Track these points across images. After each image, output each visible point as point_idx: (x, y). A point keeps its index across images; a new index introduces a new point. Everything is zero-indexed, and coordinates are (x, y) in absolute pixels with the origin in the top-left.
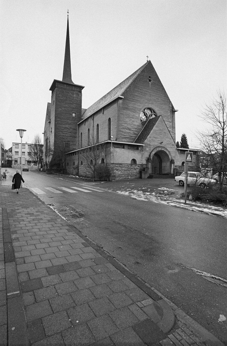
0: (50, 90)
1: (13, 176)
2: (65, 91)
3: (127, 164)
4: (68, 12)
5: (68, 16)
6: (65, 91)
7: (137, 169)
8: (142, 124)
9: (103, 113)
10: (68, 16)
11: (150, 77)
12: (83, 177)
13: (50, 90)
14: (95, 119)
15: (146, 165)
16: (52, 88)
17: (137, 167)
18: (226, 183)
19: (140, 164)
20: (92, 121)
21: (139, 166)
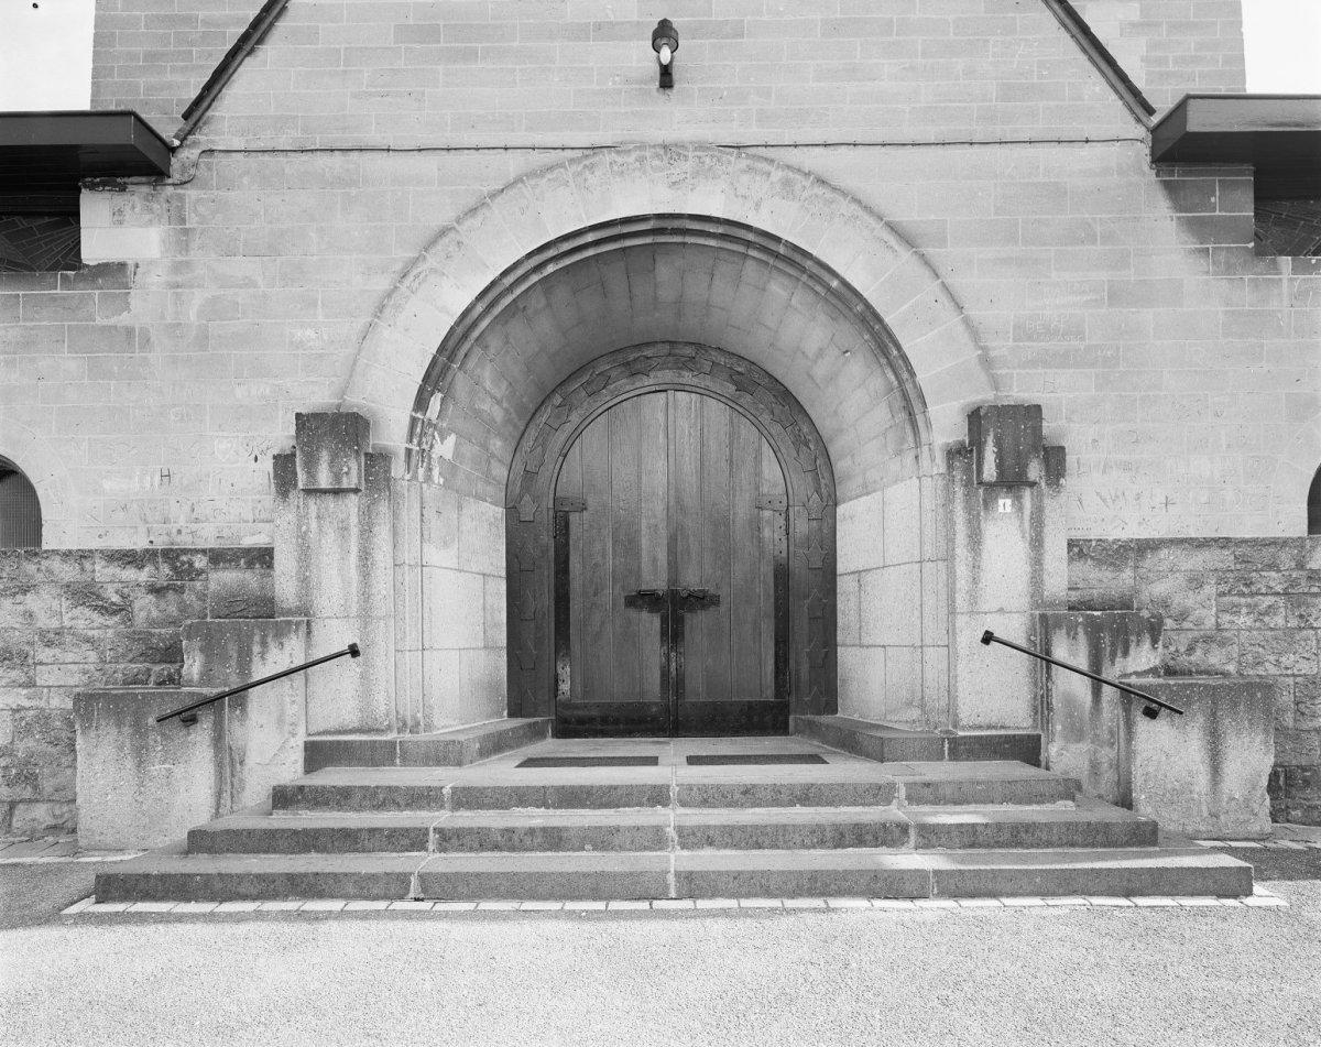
7: (52, 639)
21: (85, 594)
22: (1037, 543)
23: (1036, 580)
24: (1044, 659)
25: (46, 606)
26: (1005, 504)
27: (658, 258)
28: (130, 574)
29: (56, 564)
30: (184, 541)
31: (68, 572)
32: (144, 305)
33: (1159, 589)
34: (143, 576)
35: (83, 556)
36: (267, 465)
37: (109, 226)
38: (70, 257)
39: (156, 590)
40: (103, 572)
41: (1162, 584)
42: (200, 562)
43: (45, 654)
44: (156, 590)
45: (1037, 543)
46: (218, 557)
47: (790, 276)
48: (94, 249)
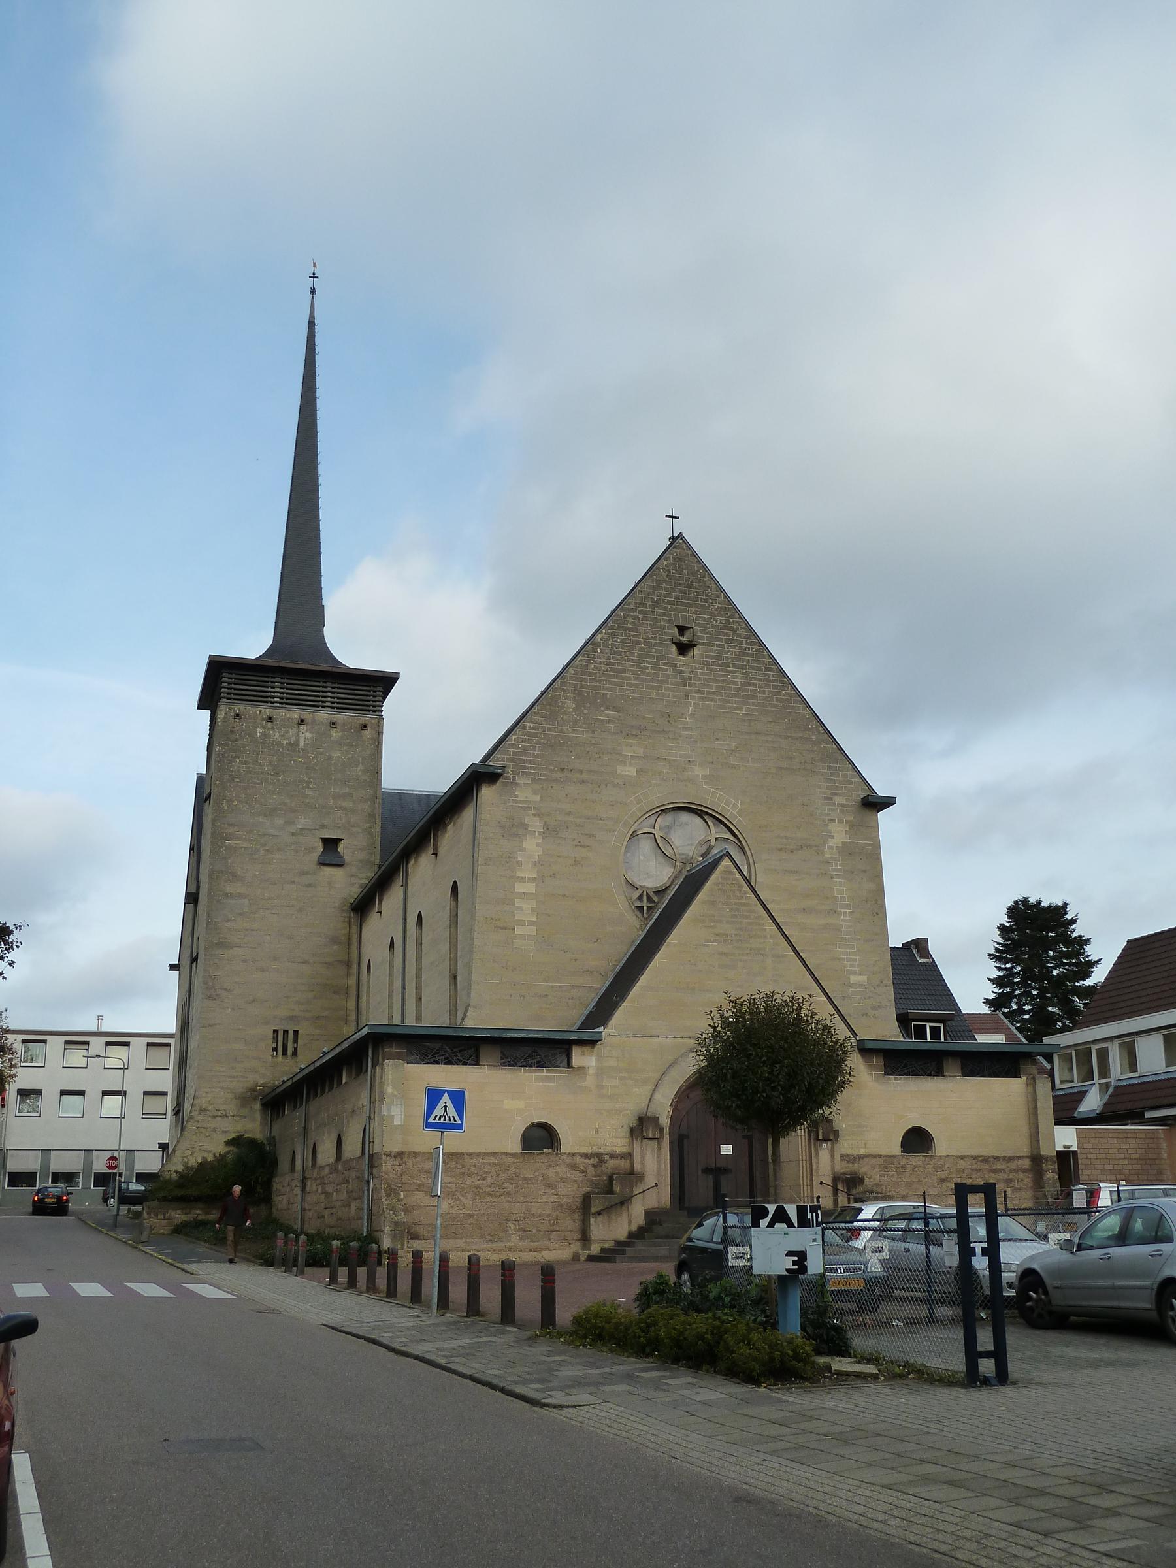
0: (201, 706)
1: (1155, 1287)
2: (288, 686)
3: (493, 1154)
4: (314, 277)
5: (313, 292)
6: (288, 686)
7: (564, 1180)
8: (640, 909)
9: (436, 854)
10: (313, 292)
11: (682, 630)
12: (985, 1252)
13: (201, 706)
14: (442, 850)
15: (623, 1156)
16: (208, 699)
17: (562, 1171)
18: (750, 1259)
19: (583, 1150)
20: (401, 890)
21: (574, 1167)
22: (833, 1156)
23: (833, 1167)
24: (836, 1191)
25: (562, 1171)
26: (824, 1145)
27: (481, 1056)
28: (587, 1161)
29: (565, 1157)
30: (601, 1151)
31: (569, 1160)
32: (590, 1081)
33: (864, 1169)
34: (591, 1162)
35: (574, 1155)
36: (628, 1130)
37: (579, 1057)
38: (569, 1066)
39: (594, 1166)
40: (579, 1160)
41: (864, 1168)
42: (607, 1157)
43: (562, 1185)
44: (594, 1166)
45: (833, 1156)
46: (612, 1156)
47: (775, 1170)
48: (575, 1062)
